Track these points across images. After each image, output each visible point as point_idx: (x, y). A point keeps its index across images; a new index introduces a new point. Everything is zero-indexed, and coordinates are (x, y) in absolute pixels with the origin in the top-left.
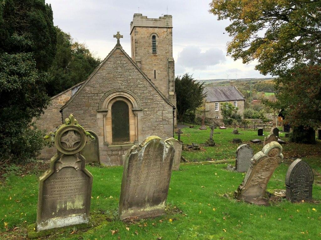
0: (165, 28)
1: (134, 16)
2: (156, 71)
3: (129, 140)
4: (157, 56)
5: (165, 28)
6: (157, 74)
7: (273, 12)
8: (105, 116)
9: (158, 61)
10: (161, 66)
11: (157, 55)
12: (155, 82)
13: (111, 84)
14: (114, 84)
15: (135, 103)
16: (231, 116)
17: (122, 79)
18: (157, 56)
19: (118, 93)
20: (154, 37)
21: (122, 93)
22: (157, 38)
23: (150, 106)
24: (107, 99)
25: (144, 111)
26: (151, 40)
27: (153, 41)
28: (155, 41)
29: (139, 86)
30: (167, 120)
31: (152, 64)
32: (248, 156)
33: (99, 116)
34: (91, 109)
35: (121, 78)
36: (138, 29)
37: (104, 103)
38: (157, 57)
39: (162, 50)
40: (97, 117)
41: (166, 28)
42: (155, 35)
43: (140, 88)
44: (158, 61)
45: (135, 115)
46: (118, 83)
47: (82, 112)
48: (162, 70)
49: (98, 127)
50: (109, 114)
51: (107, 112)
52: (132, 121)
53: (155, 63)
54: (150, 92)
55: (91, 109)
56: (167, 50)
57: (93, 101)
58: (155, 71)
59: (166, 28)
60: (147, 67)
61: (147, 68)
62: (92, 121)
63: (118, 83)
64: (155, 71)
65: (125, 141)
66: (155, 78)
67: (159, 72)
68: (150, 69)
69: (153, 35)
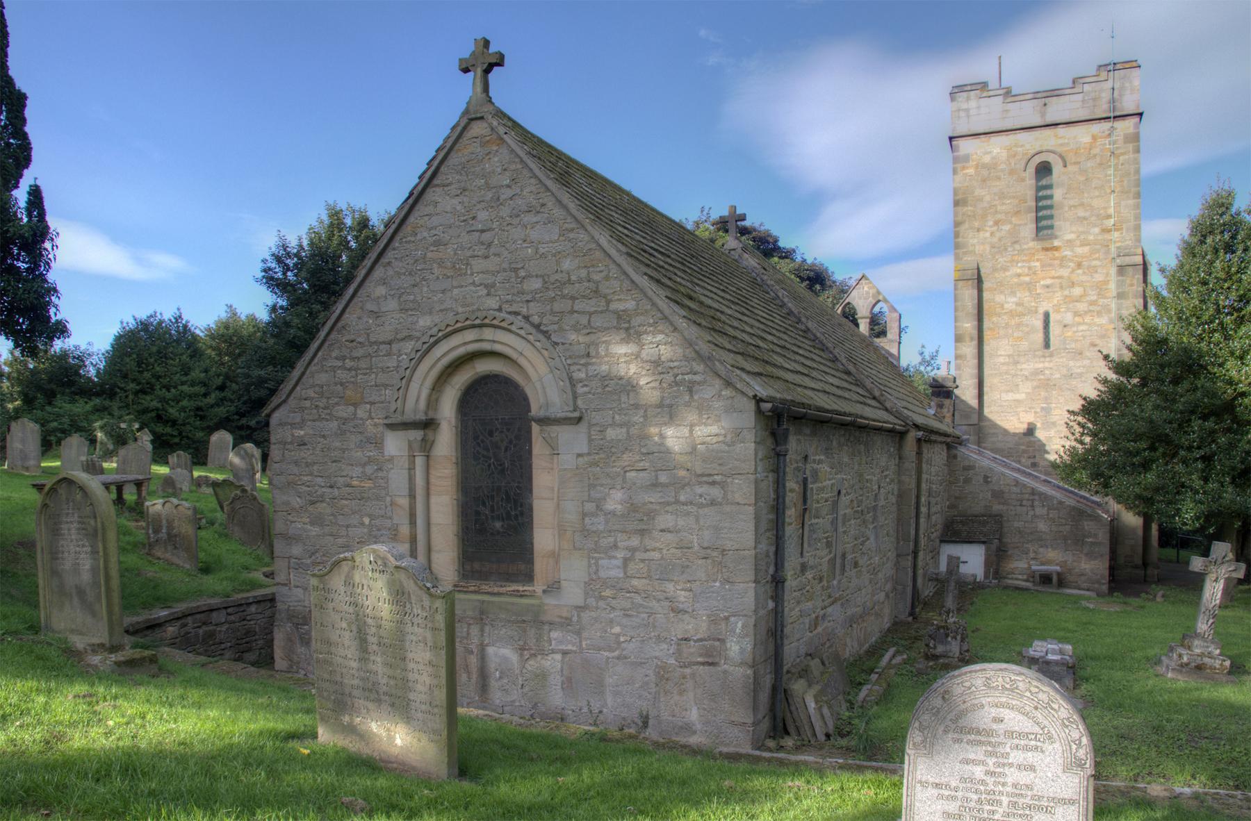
1: (953, 95)
2: (1053, 317)
3: (529, 577)
4: (1056, 249)
6: (1054, 330)
8: (426, 447)
9: (1065, 272)
10: (1077, 291)
11: (1056, 243)
12: (1047, 365)
13: (443, 292)
14: (456, 291)
17: (492, 263)
18: (1056, 249)
19: (470, 335)
20: (1044, 170)
21: (488, 333)
22: (1057, 169)
23: (624, 398)
25: (590, 426)
27: (1039, 189)
30: (718, 478)
31: (1030, 287)
32: (1025, 778)
33: (395, 444)
34: (365, 416)
35: (486, 257)
36: (965, 146)
37: (414, 386)
38: (1057, 254)
39: (1085, 218)
40: (386, 453)
42: (1050, 158)
43: (573, 298)
44: (1065, 272)
46: (473, 283)
47: (334, 425)
49: (388, 499)
50: (446, 441)
51: (428, 425)
53: (1049, 282)
55: (365, 416)
56: (1109, 217)
57: (373, 376)
58: (1047, 316)
61: (1006, 306)
62: (369, 470)
63: (473, 283)
64: (1047, 316)
65: (510, 578)
66: (1047, 345)
67: (1069, 318)
68: (1020, 309)
69: (1038, 159)
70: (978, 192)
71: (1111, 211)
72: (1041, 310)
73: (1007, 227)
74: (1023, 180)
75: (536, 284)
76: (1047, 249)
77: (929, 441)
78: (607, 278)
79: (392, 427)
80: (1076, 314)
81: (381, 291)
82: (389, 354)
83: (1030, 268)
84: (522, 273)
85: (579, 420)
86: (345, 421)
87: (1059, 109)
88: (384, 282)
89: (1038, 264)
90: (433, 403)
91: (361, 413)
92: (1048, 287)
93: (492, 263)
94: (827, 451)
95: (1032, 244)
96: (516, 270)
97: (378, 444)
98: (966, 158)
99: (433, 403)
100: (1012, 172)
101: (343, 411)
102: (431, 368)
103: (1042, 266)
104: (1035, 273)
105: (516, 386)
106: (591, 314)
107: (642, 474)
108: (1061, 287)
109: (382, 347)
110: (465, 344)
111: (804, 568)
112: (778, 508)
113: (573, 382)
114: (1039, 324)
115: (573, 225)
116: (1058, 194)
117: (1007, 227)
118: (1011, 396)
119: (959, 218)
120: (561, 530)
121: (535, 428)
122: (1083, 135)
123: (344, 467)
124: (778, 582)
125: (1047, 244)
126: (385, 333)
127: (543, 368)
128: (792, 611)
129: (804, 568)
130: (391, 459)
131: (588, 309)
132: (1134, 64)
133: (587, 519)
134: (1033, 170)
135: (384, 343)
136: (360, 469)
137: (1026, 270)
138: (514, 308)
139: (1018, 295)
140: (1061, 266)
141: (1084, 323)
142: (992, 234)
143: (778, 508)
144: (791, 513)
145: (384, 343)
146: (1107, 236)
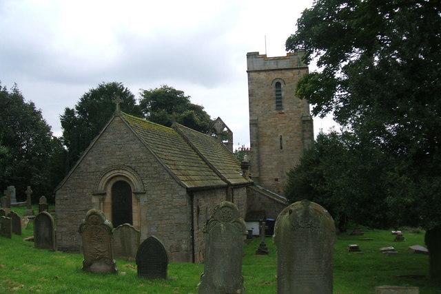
0: (295, 69)
5: (295, 69)
6: (284, 143)
7: (418, 6)
8: (103, 200)
15: (136, 185)
16: (282, 198)
19: (116, 171)
20: (278, 85)
21: (121, 171)
24: (103, 179)
26: (274, 89)
27: (277, 91)
28: (280, 91)
29: (142, 161)
31: (275, 127)
33: (95, 200)
37: (101, 184)
41: (265, 71)
42: (280, 81)
45: (138, 200)
48: (292, 134)
50: (108, 198)
51: (104, 194)
52: (135, 208)
53: (281, 125)
54: (155, 168)
59: (265, 71)
60: (269, 132)
73: (267, 105)
75: (133, 159)
77: (235, 188)
79: (94, 195)
81: (90, 158)
85: (145, 193)
88: (91, 156)
90: (105, 188)
91: (85, 191)
94: (203, 197)
97: (90, 199)
99: (105, 188)
101: (79, 190)
105: (129, 185)
111: (198, 228)
112: (192, 213)
113: (143, 184)
116: (283, 94)
117: (267, 105)
118: (270, 167)
120: (140, 220)
121: (133, 194)
122: (290, 74)
124: (193, 231)
126: (92, 169)
127: (136, 180)
128: (196, 240)
129: (198, 228)
142: (262, 107)
143: (192, 213)
144: (195, 214)
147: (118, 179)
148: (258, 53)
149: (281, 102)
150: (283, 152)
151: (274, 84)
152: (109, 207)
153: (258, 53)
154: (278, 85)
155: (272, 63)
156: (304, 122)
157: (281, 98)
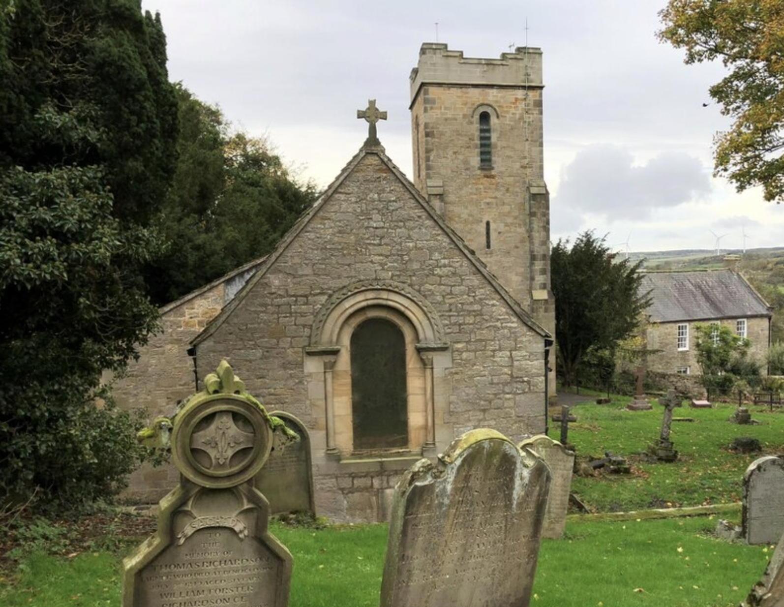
1: (423, 51)
3: (405, 442)
4: (493, 177)
6: (493, 235)
8: (330, 367)
9: (498, 194)
10: (506, 209)
11: (493, 172)
13: (349, 265)
14: (358, 265)
15: (424, 326)
17: (385, 250)
18: (493, 177)
19: (370, 295)
20: (485, 117)
21: (384, 295)
22: (493, 120)
25: (453, 352)
27: (482, 131)
28: (488, 131)
29: (438, 271)
30: (526, 379)
33: (313, 366)
34: (287, 345)
38: (493, 181)
40: (306, 371)
41: (524, 87)
42: (489, 110)
43: (441, 277)
44: (498, 194)
45: (425, 364)
47: (259, 353)
50: (344, 361)
51: (336, 353)
52: (415, 384)
53: (488, 200)
54: (471, 290)
56: (525, 158)
58: (488, 224)
59: (524, 87)
62: (291, 383)
64: (488, 224)
66: (488, 246)
67: (502, 227)
68: (471, 219)
69: (481, 110)
70: (441, 128)
71: (526, 154)
72: (485, 221)
73: (461, 157)
74: (472, 123)
76: (488, 177)
78: (461, 266)
79: (310, 354)
80: (507, 225)
82: (306, 304)
83: (477, 189)
84: (406, 258)
86: (268, 349)
87: (497, 78)
89: (481, 187)
92: (488, 204)
93: (385, 250)
95: (479, 172)
96: (402, 256)
98: (433, 101)
100: (465, 116)
102: (342, 314)
103: (485, 188)
104: (480, 193)
106: (452, 286)
107: (484, 378)
108: (497, 205)
109: (299, 299)
110: (367, 300)
114: (483, 230)
115: (440, 232)
116: (494, 137)
119: (430, 147)
123: (267, 381)
125: (487, 173)
130: (310, 375)
131: (450, 283)
132: (537, 51)
133: (452, 406)
134: (478, 117)
135: (301, 296)
136: (283, 382)
137: (474, 191)
138: (402, 279)
139: (469, 208)
140: (497, 190)
141: (511, 232)
145: (301, 296)
146: (524, 171)
147: (372, 314)
148: (446, 46)
149: (489, 153)
150: (491, 253)
151: (477, 117)
152: (346, 382)
153: (446, 46)
154: (485, 117)
155: (478, 70)
156: (534, 196)
157: (489, 145)
